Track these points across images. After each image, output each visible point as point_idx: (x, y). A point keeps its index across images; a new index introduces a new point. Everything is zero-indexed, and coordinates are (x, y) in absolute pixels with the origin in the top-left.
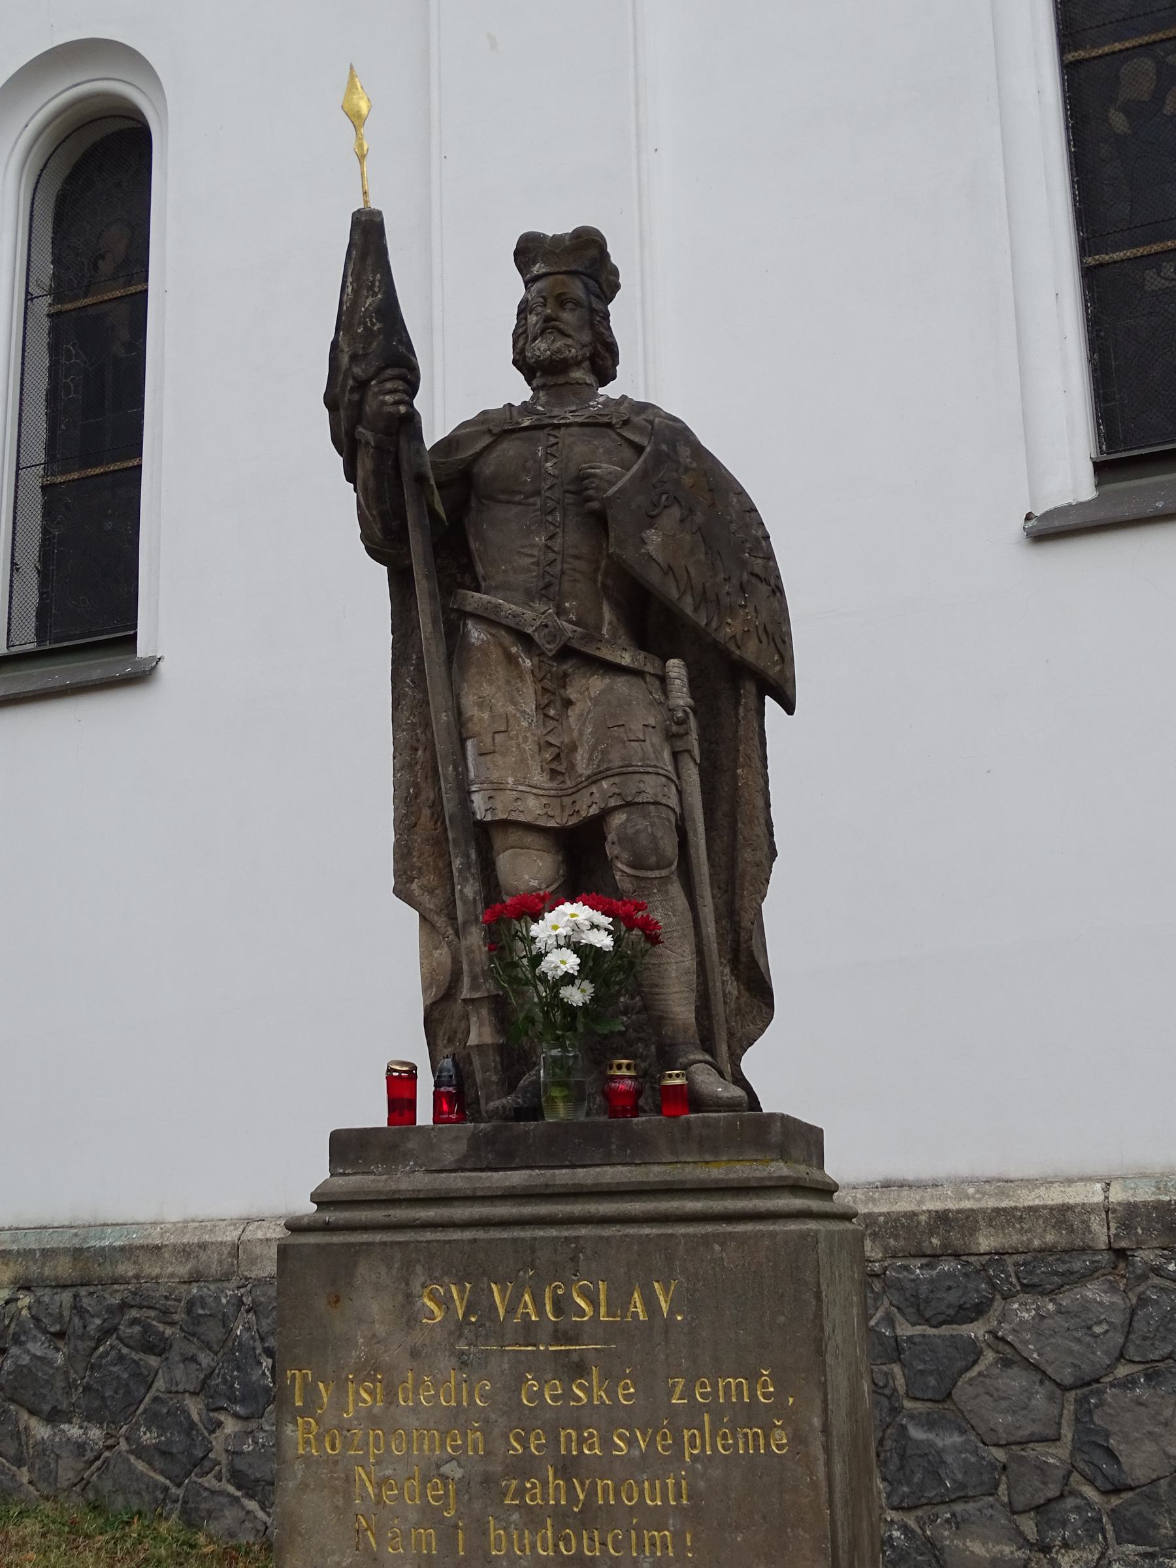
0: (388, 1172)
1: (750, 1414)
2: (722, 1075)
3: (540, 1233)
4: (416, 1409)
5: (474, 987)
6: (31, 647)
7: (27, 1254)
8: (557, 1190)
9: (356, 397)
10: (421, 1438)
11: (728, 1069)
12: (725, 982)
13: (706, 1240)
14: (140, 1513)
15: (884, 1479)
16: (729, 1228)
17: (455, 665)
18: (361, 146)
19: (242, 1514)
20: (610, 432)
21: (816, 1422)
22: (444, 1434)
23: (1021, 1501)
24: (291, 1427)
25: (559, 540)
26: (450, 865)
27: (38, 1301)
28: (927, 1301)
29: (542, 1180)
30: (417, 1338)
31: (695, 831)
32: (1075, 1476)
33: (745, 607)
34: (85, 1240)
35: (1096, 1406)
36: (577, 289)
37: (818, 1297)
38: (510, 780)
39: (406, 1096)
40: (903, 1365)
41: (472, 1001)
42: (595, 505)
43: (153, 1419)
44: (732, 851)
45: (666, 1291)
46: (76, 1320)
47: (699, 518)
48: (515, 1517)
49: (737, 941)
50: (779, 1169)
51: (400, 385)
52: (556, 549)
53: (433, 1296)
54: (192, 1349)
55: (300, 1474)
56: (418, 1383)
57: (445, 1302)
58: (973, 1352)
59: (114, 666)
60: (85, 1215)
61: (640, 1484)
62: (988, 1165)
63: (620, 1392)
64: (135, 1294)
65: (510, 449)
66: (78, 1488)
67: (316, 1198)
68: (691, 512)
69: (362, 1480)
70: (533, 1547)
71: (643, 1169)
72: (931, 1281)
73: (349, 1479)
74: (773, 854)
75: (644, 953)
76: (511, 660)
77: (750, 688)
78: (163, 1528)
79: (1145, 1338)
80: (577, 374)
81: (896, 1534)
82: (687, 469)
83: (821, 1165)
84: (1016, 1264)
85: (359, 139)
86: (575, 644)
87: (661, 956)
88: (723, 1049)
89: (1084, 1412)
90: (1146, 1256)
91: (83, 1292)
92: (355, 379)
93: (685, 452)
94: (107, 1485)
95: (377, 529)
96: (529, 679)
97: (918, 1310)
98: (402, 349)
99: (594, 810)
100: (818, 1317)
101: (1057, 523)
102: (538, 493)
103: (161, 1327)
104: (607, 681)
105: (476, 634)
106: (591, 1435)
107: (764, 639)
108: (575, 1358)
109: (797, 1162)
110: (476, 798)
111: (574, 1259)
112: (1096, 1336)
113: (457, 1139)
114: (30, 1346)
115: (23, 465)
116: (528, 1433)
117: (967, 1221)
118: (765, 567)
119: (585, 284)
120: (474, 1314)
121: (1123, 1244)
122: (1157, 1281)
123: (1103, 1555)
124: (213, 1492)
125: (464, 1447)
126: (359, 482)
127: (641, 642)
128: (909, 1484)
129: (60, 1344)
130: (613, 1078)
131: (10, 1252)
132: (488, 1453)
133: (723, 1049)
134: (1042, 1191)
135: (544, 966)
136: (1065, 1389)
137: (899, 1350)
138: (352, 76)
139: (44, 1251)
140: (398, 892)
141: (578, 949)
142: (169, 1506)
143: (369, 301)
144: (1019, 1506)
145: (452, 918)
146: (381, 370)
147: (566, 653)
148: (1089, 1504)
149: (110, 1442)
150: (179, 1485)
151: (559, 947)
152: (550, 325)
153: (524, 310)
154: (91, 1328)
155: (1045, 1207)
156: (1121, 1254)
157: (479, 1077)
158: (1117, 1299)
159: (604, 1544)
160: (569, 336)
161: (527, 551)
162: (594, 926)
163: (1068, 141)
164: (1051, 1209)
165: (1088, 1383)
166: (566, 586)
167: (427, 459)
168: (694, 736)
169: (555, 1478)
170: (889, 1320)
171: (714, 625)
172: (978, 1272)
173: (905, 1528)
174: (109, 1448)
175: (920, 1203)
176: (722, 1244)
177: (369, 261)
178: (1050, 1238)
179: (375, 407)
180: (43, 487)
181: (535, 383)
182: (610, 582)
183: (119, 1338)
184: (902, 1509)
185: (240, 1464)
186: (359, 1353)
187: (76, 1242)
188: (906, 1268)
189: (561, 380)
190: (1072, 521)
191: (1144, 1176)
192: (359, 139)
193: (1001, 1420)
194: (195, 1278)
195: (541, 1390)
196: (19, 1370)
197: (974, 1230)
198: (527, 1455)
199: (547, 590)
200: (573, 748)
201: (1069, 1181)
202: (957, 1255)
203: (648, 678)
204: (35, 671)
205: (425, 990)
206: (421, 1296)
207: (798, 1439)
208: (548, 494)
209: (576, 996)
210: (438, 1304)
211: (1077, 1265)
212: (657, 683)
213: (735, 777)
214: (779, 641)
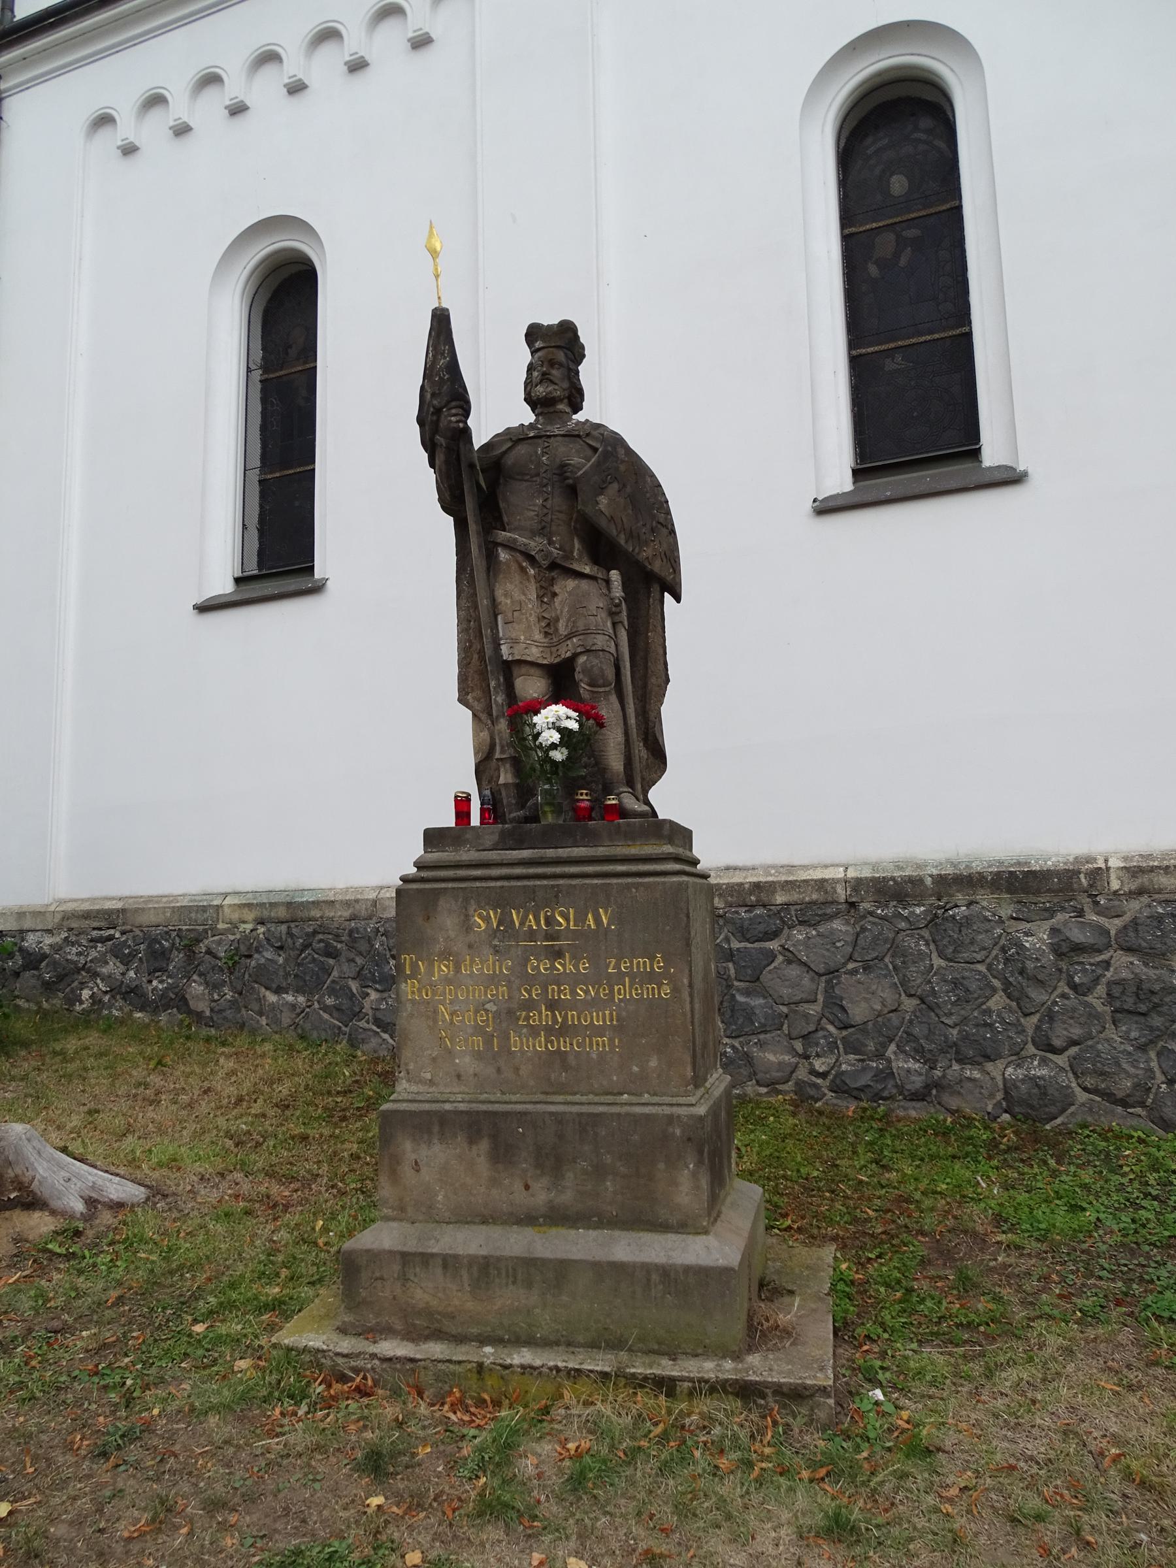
0: (456, 851)
1: (651, 977)
2: (638, 799)
3: (538, 883)
5: (502, 752)
6: (256, 572)
7: (262, 905)
8: (547, 860)
9: (435, 418)
10: (474, 990)
11: (641, 797)
12: (640, 751)
13: (628, 887)
14: (326, 1040)
15: (723, 1022)
16: (640, 880)
17: (491, 573)
18: (437, 269)
19: (380, 1041)
20: (578, 439)
21: (686, 981)
22: (486, 988)
23: (794, 1034)
24: (404, 985)
25: (550, 502)
26: (489, 685)
27: (269, 930)
28: (748, 930)
29: (539, 855)
30: (471, 938)
31: (625, 667)
32: (824, 1020)
33: (654, 541)
34: (293, 898)
35: (836, 984)
36: (561, 356)
37: (688, 917)
38: (522, 637)
39: (465, 810)
40: (734, 963)
41: (501, 759)
42: (570, 481)
43: (332, 992)
44: (645, 677)
45: (606, 913)
46: (289, 940)
47: (628, 489)
48: (525, 1030)
49: (647, 728)
50: (668, 849)
51: (460, 411)
52: (548, 507)
53: (480, 916)
54: (352, 955)
55: (409, 1009)
56: (472, 961)
57: (487, 919)
58: (771, 956)
59: (292, 584)
60: (293, 885)
61: (591, 1014)
62: (783, 858)
63: (581, 966)
64: (320, 926)
65: (522, 450)
66: (293, 1027)
67: (416, 864)
68: (624, 486)
70: (534, 1046)
71: (594, 849)
72: (750, 919)
73: (435, 1012)
74: (668, 681)
75: (596, 733)
76: (523, 570)
77: (656, 588)
78: (338, 1048)
79: (863, 949)
80: (561, 407)
81: (728, 1050)
82: (623, 462)
83: (691, 850)
84: (796, 910)
85: (436, 265)
86: (558, 561)
87: (603, 734)
88: (639, 786)
89: (830, 987)
90: (865, 906)
91: (293, 925)
92: (434, 407)
93: (621, 451)
94: (308, 1026)
95: (447, 495)
96: (533, 580)
97: (743, 934)
98: (461, 390)
99: (569, 654)
100: (688, 926)
101: (831, 504)
102: (538, 475)
103: (335, 944)
104: (577, 582)
105: (503, 555)
106: (565, 989)
107: (665, 560)
108: (557, 948)
109: (677, 846)
110: (503, 647)
111: (556, 896)
112: (838, 948)
113: (493, 833)
114: (265, 954)
115: (247, 468)
116: (531, 988)
117: (771, 887)
118: (666, 519)
119: (566, 355)
120: (502, 925)
121: (854, 900)
122: (871, 919)
123: (837, 1060)
124: (364, 1029)
126: (437, 468)
127: (596, 560)
128: (736, 1024)
129: (281, 953)
130: (579, 800)
131: (252, 904)
132: (509, 997)
133: (639, 786)
134: (811, 872)
135: (541, 739)
136: (820, 975)
137: (732, 955)
138: (431, 227)
139: (271, 904)
140: (460, 700)
141: (560, 730)
142: (342, 1036)
143: (442, 361)
144: (793, 1036)
145: (490, 714)
146: (448, 402)
147: (554, 566)
148: (831, 1035)
149: (309, 1004)
150: (346, 1026)
151: (549, 728)
152: (545, 378)
153: (530, 368)
154: (298, 944)
155: (812, 880)
156: (852, 905)
157: (505, 802)
158: (849, 928)
159: (571, 1044)
160: (556, 384)
161: (531, 508)
162: (568, 717)
163: (844, 282)
164: (816, 881)
165: (832, 972)
166: (554, 528)
167: (476, 455)
168: (625, 613)
169: (546, 1010)
170: (727, 940)
171: (637, 550)
172: (775, 914)
173: (733, 1047)
174: (309, 1007)
175: (745, 878)
176: (636, 889)
177: (442, 338)
178: (815, 896)
179: (446, 424)
180: (260, 481)
181: (536, 412)
182: (578, 526)
183: (313, 949)
184: (732, 1037)
185: (379, 1015)
186: (438, 947)
187: (288, 899)
188: (737, 912)
189: (552, 410)
190: (839, 503)
191: (866, 864)
192: (436, 265)
193: (785, 991)
194: (353, 918)
195: (538, 966)
196: (259, 966)
197: (774, 892)
198: (531, 999)
199: (543, 530)
200: (557, 620)
201: (826, 867)
202: (764, 906)
203: (600, 581)
204: (257, 586)
205: (475, 754)
206: (473, 916)
207: (676, 990)
208: (544, 475)
209: (558, 755)
211: (829, 911)
212: (604, 584)
213: (647, 637)
214: (673, 562)
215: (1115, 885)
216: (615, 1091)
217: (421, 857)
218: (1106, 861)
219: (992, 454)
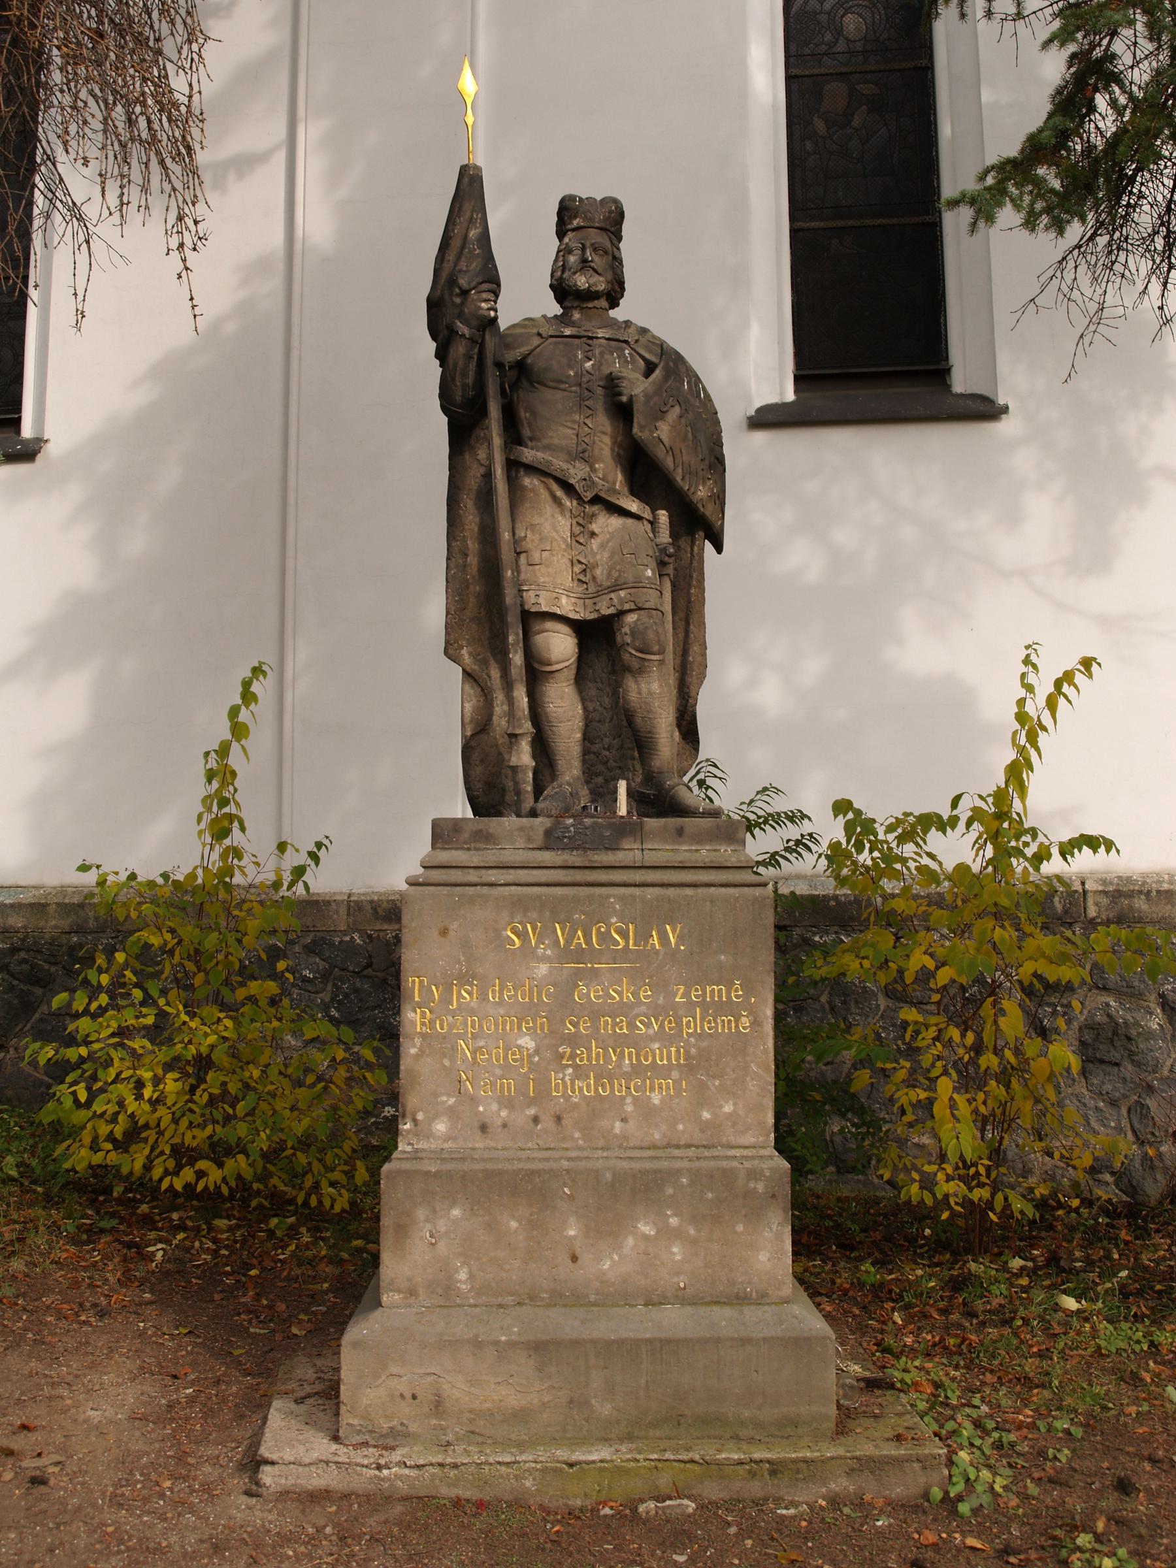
4: (501, 1002)
13: (590, 897)
45: (674, 931)
53: (514, 931)
63: (693, 993)
69: (462, 1049)
73: (454, 1048)
86: (602, 494)
99: (612, 611)
106: (622, 1021)
125: (534, 1028)
171: (692, 490)
194: (79, 930)
203: (646, 523)
210: (518, 936)
215: (1092, 912)
216: (682, 1143)
217: (427, 856)
218: (1083, 883)
219: (960, 383)
